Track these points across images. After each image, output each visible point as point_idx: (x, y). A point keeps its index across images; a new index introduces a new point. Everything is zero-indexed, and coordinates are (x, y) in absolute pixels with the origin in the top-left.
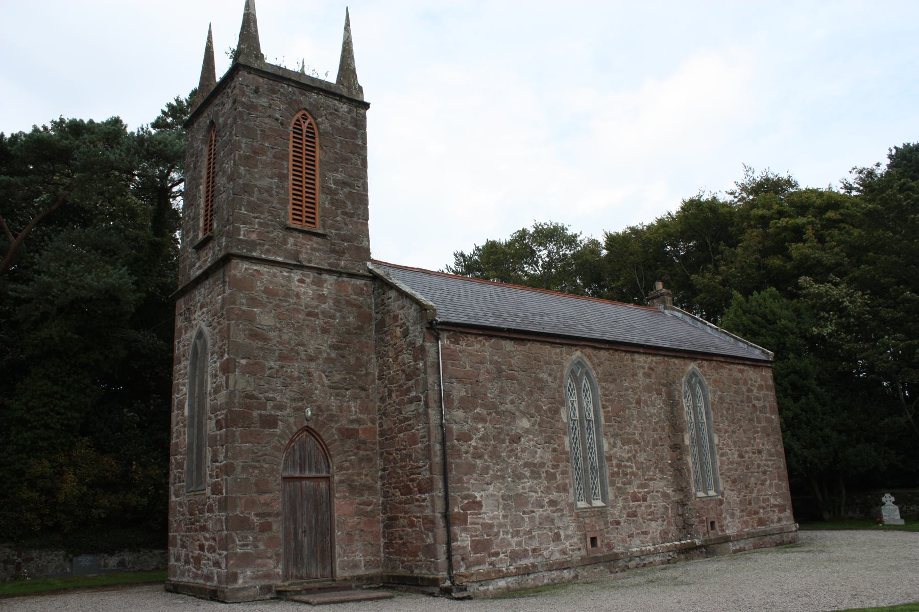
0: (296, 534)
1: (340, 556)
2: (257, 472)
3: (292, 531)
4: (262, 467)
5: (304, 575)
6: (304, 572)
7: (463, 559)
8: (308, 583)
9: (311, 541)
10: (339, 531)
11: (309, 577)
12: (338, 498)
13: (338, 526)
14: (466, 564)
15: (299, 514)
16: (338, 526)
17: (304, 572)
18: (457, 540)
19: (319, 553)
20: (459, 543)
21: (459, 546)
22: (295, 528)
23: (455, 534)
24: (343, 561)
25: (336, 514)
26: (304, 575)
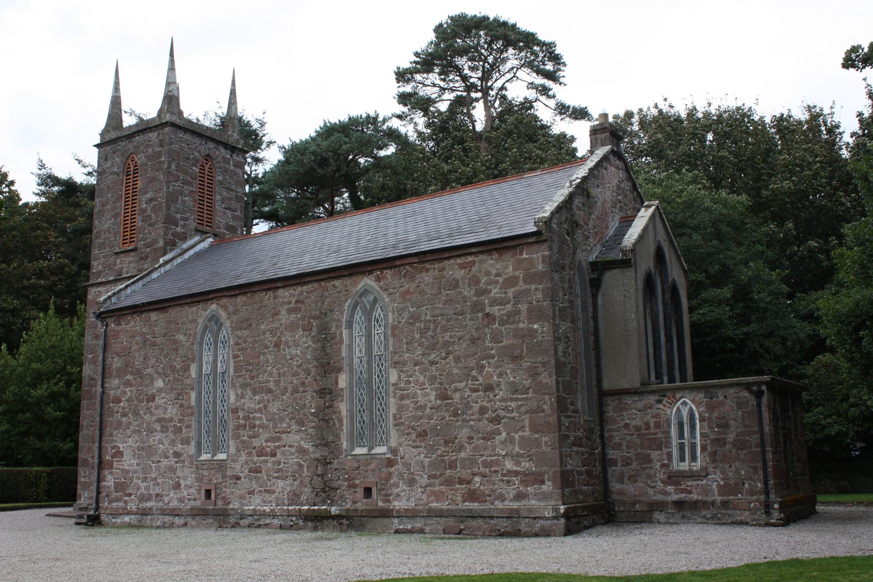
18: (105, 481)
23: (105, 476)
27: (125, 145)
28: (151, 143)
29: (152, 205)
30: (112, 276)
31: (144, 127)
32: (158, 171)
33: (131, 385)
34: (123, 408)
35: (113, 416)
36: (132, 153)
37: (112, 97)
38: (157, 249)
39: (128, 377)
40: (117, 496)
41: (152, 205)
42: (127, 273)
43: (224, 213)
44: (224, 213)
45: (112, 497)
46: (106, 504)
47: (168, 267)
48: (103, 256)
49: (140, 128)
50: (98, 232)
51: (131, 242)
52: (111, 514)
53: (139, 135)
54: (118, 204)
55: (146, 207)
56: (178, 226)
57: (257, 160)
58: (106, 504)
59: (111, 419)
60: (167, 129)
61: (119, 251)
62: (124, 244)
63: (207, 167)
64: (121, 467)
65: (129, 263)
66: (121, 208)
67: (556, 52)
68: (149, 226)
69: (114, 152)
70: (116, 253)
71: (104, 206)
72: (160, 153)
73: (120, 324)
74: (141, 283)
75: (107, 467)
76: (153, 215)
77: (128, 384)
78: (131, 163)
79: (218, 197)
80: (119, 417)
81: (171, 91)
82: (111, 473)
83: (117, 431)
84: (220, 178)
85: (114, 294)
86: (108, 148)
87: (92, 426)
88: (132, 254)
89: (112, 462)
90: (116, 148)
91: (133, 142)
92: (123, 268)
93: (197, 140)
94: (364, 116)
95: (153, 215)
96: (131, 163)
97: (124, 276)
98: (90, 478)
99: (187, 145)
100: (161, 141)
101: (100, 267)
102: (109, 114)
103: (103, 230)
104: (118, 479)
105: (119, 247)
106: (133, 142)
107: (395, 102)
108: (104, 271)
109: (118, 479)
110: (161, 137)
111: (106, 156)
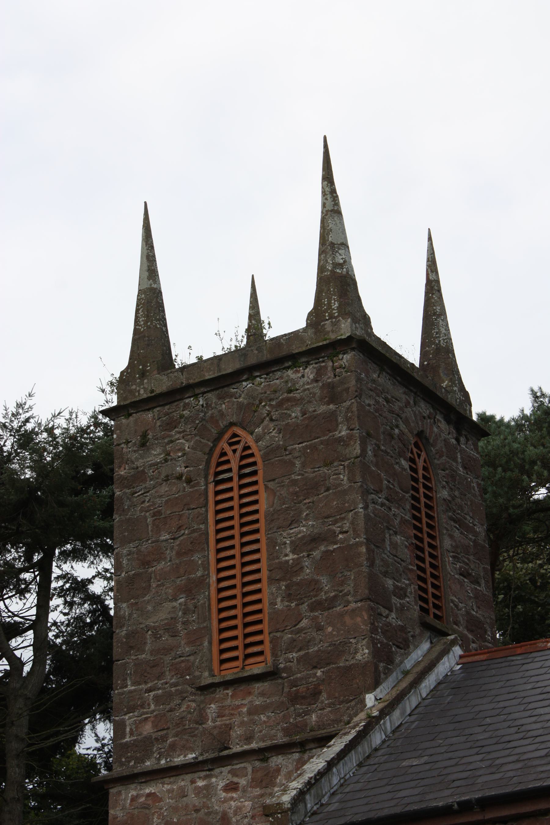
27: (208, 406)
28: (297, 395)
29: (316, 554)
30: (193, 750)
31: (266, 356)
32: (328, 464)
36: (232, 424)
37: (140, 291)
38: (348, 669)
41: (316, 554)
42: (249, 739)
43: (461, 584)
44: (461, 584)
47: (396, 718)
48: (157, 699)
49: (252, 360)
50: (131, 635)
51: (247, 656)
53: (251, 378)
54: (197, 557)
55: (297, 562)
56: (391, 610)
57: (103, 557)
60: (346, 359)
61: (210, 681)
62: (222, 662)
63: (420, 463)
65: (250, 713)
66: (206, 567)
68: (312, 608)
69: (171, 425)
70: (204, 689)
71: (146, 564)
72: (331, 418)
74: (354, 758)
76: (324, 580)
78: (228, 450)
79: (447, 543)
81: (341, 266)
84: (445, 494)
85: (310, 785)
86: (149, 415)
90: (176, 415)
91: (232, 395)
92: (230, 727)
93: (399, 392)
94: (498, 418)
95: (324, 580)
96: (228, 450)
97: (237, 749)
99: (387, 401)
100: (331, 387)
101: (148, 729)
102: (136, 332)
103: (148, 628)
105: (211, 670)
106: (232, 395)
108: (164, 739)
110: (329, 377)
111: (144, 435)
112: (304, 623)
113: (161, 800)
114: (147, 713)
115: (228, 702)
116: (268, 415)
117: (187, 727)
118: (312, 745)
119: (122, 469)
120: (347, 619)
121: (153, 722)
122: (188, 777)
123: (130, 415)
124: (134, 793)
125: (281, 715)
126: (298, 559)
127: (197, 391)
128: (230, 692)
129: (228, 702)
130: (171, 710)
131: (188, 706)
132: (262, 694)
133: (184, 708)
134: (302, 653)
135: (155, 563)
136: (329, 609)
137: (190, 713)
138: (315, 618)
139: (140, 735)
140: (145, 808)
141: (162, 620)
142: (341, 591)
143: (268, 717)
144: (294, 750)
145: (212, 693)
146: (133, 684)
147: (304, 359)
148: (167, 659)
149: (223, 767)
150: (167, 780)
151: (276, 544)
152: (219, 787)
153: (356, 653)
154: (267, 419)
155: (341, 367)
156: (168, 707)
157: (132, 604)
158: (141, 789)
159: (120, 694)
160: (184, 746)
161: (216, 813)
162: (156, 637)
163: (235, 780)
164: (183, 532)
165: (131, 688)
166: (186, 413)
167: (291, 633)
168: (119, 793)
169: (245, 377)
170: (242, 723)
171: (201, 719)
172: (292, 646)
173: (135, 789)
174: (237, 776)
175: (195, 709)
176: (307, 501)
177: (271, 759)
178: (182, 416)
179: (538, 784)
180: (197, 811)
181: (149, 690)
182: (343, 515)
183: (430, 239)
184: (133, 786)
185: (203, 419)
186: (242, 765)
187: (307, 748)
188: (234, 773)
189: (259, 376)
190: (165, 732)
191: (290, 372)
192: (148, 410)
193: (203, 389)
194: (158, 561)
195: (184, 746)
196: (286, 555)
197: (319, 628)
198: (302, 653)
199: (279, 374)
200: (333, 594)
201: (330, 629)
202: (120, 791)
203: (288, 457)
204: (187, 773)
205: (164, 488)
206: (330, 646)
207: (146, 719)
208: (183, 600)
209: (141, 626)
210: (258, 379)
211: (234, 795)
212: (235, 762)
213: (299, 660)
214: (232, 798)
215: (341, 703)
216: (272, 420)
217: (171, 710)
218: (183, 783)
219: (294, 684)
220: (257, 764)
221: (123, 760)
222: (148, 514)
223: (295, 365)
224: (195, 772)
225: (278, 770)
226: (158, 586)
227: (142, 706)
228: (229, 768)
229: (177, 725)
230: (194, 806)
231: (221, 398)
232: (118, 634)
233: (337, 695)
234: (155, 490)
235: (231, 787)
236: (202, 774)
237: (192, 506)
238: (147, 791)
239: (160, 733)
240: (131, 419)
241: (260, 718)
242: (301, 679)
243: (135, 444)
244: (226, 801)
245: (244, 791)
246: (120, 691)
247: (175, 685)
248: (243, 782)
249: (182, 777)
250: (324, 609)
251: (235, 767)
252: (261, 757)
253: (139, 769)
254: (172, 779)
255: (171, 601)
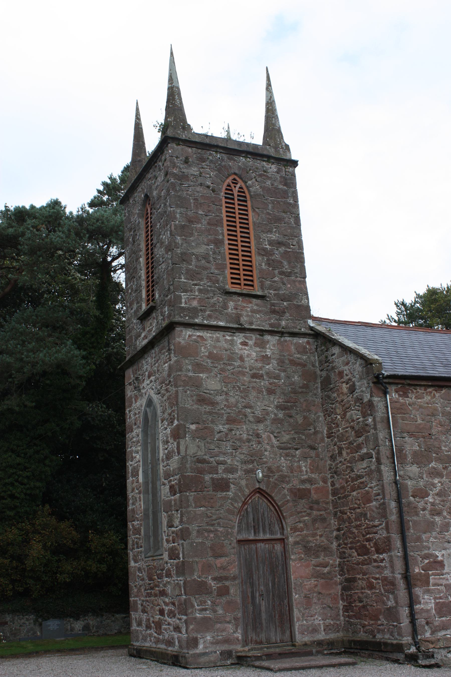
0: (253, 597)
1: (298, 620)
2: (212, 535)
3: (250, 595)
4: (217, 530)
5: (264, 640)
6: (263, 636)
7: (427, 623)
8: (267, 648)
9: (269, 605)
10: (296, 594)
11: (268, 642)
12: (294, 560)
13: (295, 588)
14: (431, 628)
15: (255, 577)
16: (295, 588)
17: (263, 636)
18: (420, 603)
19: (277, 617)
20: (422, 606)
21: (422, 609)
22: (252, 592)
23: (418, 596)
24: (302, 625)
25: (292, 577)
26: (264, 640)
33: (439, 474)
34: (433, 504)
35: (417, 514)
39: (433, 464)
40: (442, 621)
45: (436, 624)
46: (428, 635)
52: (444, 648)
53: (246, 157)
58: (428, 635)
59: (415, 518)
64: (444, 582)
67: (12, 209)
69: (202, 160)
71: (190, 221)
73: (405, 395)
75: (419, 583)
77: (435, 473)
80: (428, 516)
82: (428, 591)
83: (428, 535)
87: (211, 531)
88: (259, 301)
89: (428, 576)
90: (205, 156)
91: (235, 160)
98: (215, 611)
101: (195, 303)
104: (440, 598)
107: (69, 211)
108: (205, 311)
109: (440, 598)
112: (276, 279)
113: (206, 340)
114: (194, 295)
115: (240, 303)
116: (255, 178)
117: (217, 308)
118: (287, 335)
119: (175, 169)
120: (297, 284)
121: (198, 301)
122: (222, 333)
123: (179, 145)
124: (191, 333)
125: (267, 317)
126: (272, 249)
127: (218, 150)
128: (240, 299)
129: (240, 303)
130: (208, 298)
131: (218, 299)
132: (257, 305)
133: (215, 299)
134: (276, 292)
135: (195, 223)
136: (288, 276)
137: (219, 302)
138: (281, 279)
139: (190, 305)
140: (196, 342)
141: (201, 253)
142: (293, 271)
143: (261, 316)
144: (278, 335)
145: (231, 296)
146: (185, 279)
147: (272, 161)
148: (205, 272)
149: (240, 333)
150: (209, 331)
151: (260, 238)
152: (238, 342)
153: (302, 300)
154: (254, 179)
155: (289, 172)
156: (206, 296)
157: (183, 238)
158: (194, 332)
159: (178, 281)
160: (217, 317)
161: (237, 354)
162: (197, 258)
163: (247, 341)
164: (211, 214)
165: (183, 280)
166: (210, 158)
167: (270, 281)
168: (182, 331)
169: (243, 155)
170: (248, 316)
171: (225, 307)
172: (270, 288)
173: (191, 331)
174: (247, 339)
175: (221, 302)
176: (275, 225)
177: (265, 336)
178: (208, 158)
179: (446, 375)
180: (226, 350)
181: (196, 285)
182: (293, 238)
183: (137, 103)
184: (190, 330)
185: (220, 165)
186: (250, 335)
187: (284, 335)
188: (246, 337)
189: (249, 158)
190: (204, 308)
191: (264, 163)
192: (189, 147)
193: (221, 151)
194: (198, 223)
195: (217, 317)
196: (266, 245)
197: (284, 284)
198: (276, 292)
199: (259, 161)
200: (289, 271)
201: (289, 286)
202: (182, 330)
203: (265, 201)
204: (221, 331)
205: (199, 189)
206: (290, 293)
207: (194, 298)
208: (212, 247)
209: (189, 252)
210: (248, 159)
211: (246, 348)
212: (248, 332)
213: (275, 295)
214: (245, 349)
215: (296, 320)
216: (256, 180)
217: (208, 298)
218: (218, 335)
219: (273, 305)
220: (258, 336)
221: (182, 315)
222: (191, 198)
223: (268, 161)
224: (225, 332)
225: (268, 342)
226: (198, 235)
227: (191, 291)
228: (243, 334)
229: (212, 306)
230: (225, 348)
231: (230, 159)
232: (175, 251)
233: (294, 316)
234: (194, 187)
235: (244, 344)
236: (229, 334)
237: (216, 203)
238: (198, 334)
239: (202, 308)
240: (179, 147)
241: (257, 316)
242: (277, 304)
243: (181, 160)
244: (241, 349)
245: (251, 347)
246: (178, 280)
247: (210, 287)
248: (251, 343)
249: (218, 332)
250: (286, 276)
251: (246, 335)
252: (261, 334)
253: (191, 321)
254: (212, 332)
255: (205, 245)
